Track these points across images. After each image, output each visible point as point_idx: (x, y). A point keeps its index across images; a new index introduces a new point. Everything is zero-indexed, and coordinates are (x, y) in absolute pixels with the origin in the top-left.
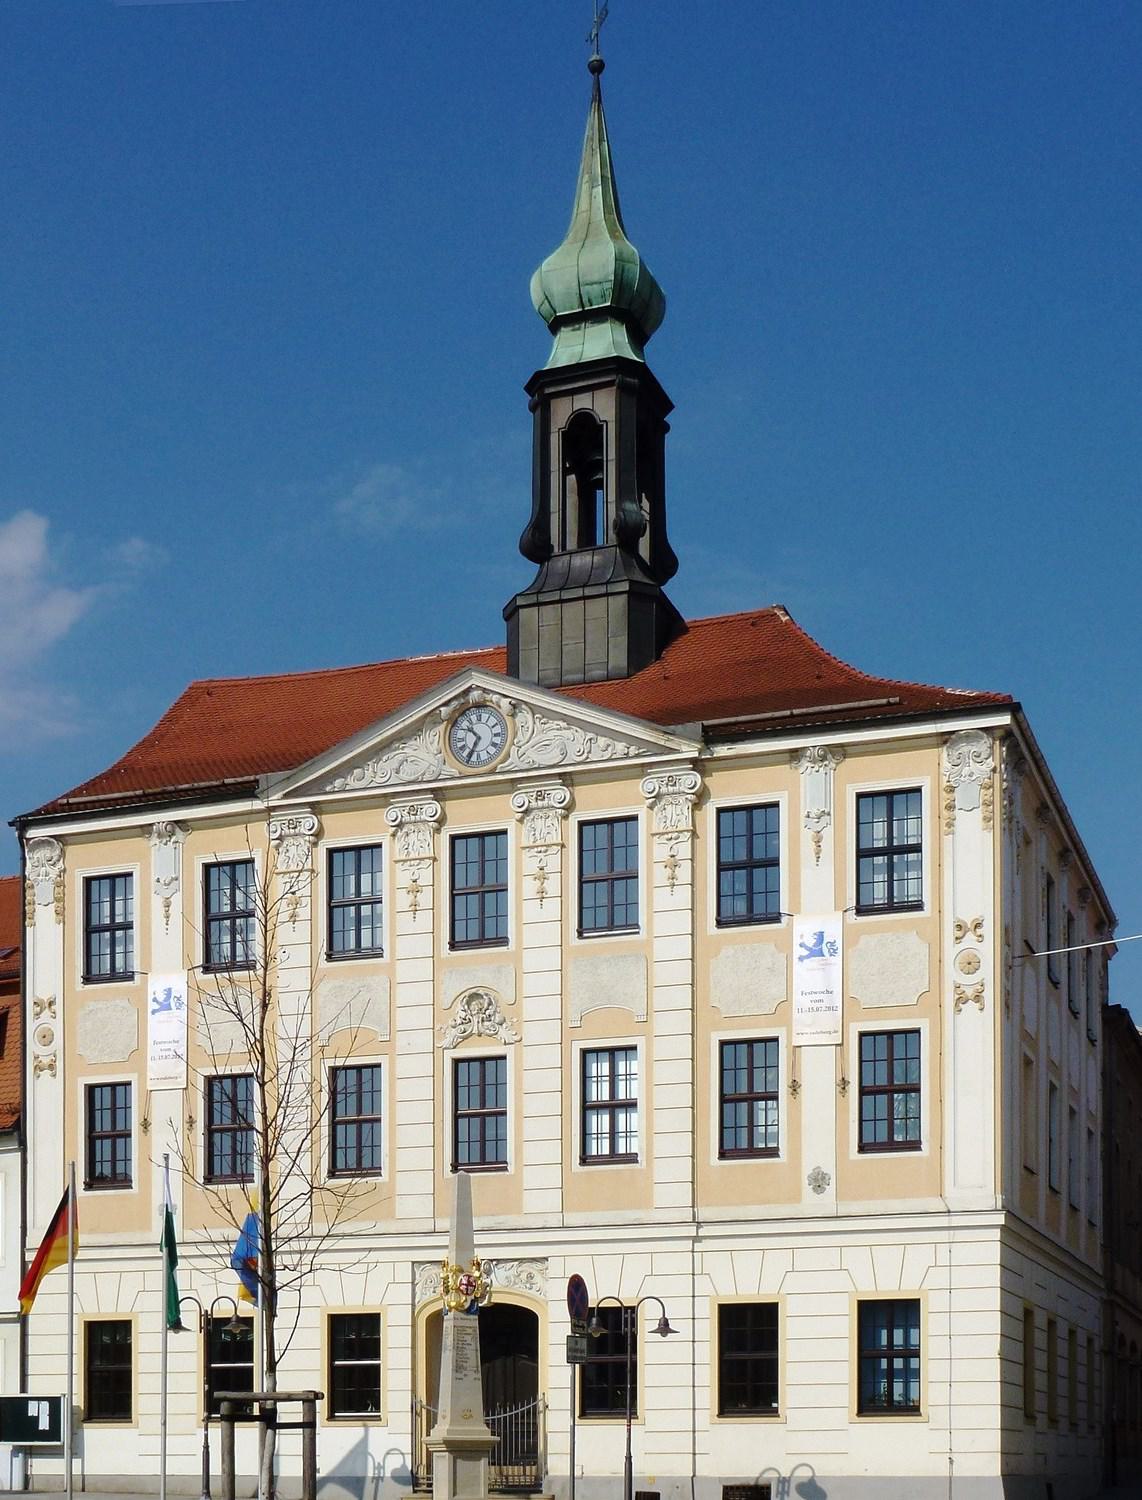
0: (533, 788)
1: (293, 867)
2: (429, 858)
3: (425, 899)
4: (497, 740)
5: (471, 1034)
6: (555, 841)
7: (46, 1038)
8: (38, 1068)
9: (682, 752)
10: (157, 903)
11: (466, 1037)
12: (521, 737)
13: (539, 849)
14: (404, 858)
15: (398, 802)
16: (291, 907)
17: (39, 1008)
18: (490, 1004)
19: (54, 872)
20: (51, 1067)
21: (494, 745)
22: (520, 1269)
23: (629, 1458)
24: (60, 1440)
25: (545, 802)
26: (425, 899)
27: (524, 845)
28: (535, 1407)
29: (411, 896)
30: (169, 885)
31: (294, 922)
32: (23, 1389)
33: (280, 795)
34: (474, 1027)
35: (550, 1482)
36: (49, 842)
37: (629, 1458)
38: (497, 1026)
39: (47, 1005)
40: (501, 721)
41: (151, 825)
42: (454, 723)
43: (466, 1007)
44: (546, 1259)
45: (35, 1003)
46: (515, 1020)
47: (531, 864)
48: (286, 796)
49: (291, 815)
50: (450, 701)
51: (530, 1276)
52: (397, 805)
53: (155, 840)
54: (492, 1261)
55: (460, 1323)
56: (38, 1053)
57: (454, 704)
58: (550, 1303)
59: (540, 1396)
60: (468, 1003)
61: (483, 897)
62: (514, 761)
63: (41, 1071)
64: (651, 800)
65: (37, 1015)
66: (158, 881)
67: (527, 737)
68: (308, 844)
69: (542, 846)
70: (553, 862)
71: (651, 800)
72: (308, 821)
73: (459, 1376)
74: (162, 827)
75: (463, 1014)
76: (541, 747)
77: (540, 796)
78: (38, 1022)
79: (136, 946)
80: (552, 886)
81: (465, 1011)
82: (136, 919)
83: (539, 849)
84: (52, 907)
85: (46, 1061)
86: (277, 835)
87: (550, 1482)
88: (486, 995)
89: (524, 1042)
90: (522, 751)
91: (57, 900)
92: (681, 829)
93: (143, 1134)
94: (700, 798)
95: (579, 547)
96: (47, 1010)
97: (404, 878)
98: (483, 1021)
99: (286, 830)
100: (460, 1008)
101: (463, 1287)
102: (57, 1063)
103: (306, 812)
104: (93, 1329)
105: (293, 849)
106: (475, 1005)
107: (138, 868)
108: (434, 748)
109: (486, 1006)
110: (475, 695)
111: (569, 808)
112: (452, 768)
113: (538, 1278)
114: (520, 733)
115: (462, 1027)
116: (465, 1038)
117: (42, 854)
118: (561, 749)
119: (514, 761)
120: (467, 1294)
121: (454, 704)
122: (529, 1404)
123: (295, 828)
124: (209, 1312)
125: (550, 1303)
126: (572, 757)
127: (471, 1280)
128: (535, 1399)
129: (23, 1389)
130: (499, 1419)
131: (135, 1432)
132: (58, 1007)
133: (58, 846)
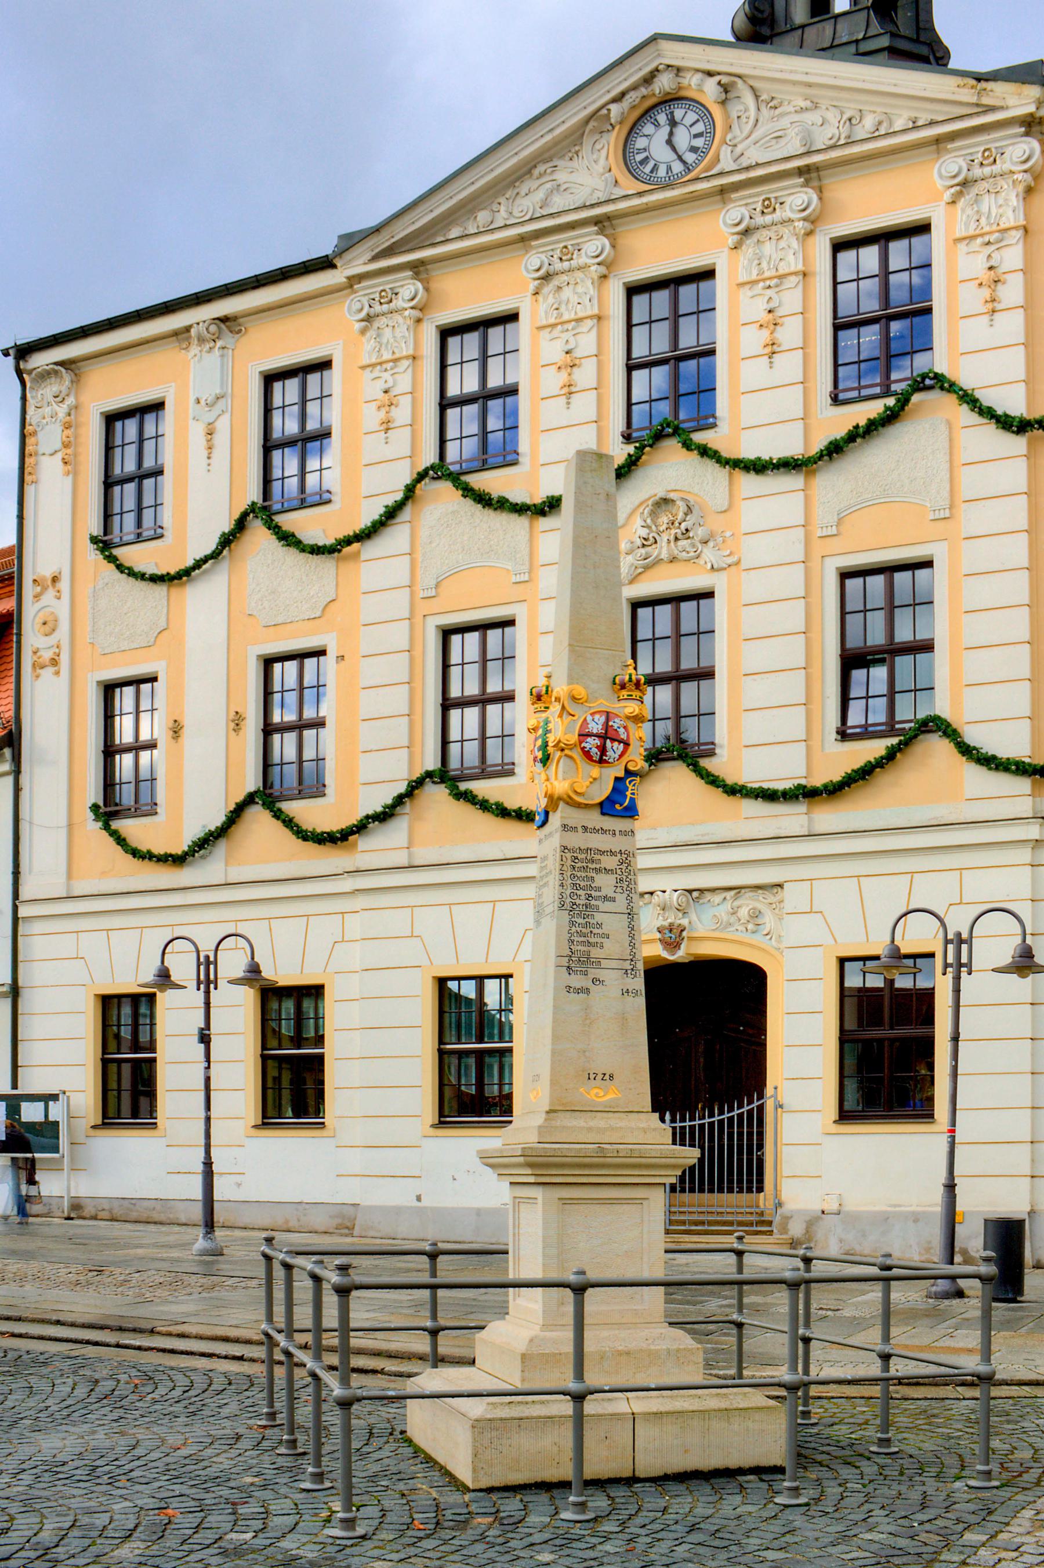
0: (756, 196)
1: (387, 356)
2: (795, 273)
3: (586, 375)
4: (699, 142)
5: (658, 561)
6: (793, 269)
7: (49, 626)
8: (37, 666)
9: (1007, 108)
10: (197, 433)
11: (649, 566)
12: (738, 132)
13: (768, 283)
14: (552, 321)
15: (544, 245)
16: (383, 411)
17: (39, 589)
18: (689, 510)
19: (62, 410)
20: (54, 662)
21: (694, 149)
22: (736, 903)
23: (950, 1187)
24: (58, 1152)
25: (778, 216)
26: (586, 375)
27: (741, 280)
28: (761, 1109)
29: (564, 374)
30: (212, 405)
31: (387, 430)
32: (15, 1086)
33: (368, 256)
34: (663, 550)
35: (787, 1219)
36: (56, 372)
37: (950, 1187)
38: (700, 546)
39: (49, 582)
40: (705, 113)
41: (188, 329)
42: (633, 130)
43: (649, 521)
44: (780, 886)
45: (35, 581)
46: (728, 534)
47: (754, 307)
48: (375, 258)
49: (385, 282)
50: (623, 94)
51: (756, 915)
52: (541, 250)
53: (195, 349)
54: (690, 891)
55: (577, 840)
56: (37, 645)
57: (632, 97)
58: (786, 952)
59: (769, 1091)
60: (654, 514)
61: (676, 369)
62: (726, 163)
63: (42, 668)
64: (953, 190)
65: (37, 597)
66: (198, 401)
67: (745, 133)
68: (408, 322)
69: (770, 278)
70: (791, 299)
71: (953, 190)
72: (409, 288)
73: (577, 981)
74: (202, 327)
75: (644, 532)
76: (769, 141)
77: (768, 207)
78: (38, 605)
79: (168, 495)
80: (790, 333)
81: (649, 527)
82: (168, 460)
83: (768, 283)
84: (59, 456)
85: (47, 655)
86: (363, 314)
87: (787, 1219)
88: (683, 499)
89: (744, 565)
90: (739, 150)
91: (66, 445)
92: (1007, 226)
93: (174, 741)
94: (608, 267)
95: (812, 17)
96: (51, 587)
97: (552, 350)
98: (676, 539)
99: (378, 308)
100: (639, 522)
101: (592, 743)
102: (62, 656)
103: (404, 279)
104: (108, 1002)
105: (387, 333)
106: (664, 520)
107: (172, 390)
108: (600, 167)
109: (680, 516)
110: (665, 83)
111: (814, 221)
112: (630, 186)
113: (769, 920)
114: (735, 127)
115: (643, 551)
116: (647, 568)
117: (50, 389)
118: (803, 138)
119: (726, 163)
120: (601, 761)
121: (632, 97)
122: (750, 1102)
123: (391, 301)
124: (212, 959)
125: (786, 952)
126: (821, 140)
127: (616, 723)
128: (761, 1096)
129: (15, 1086)
130: (692, 1127)
131: (163, 1141)
132: (64, 585)
133: (67, 376)
